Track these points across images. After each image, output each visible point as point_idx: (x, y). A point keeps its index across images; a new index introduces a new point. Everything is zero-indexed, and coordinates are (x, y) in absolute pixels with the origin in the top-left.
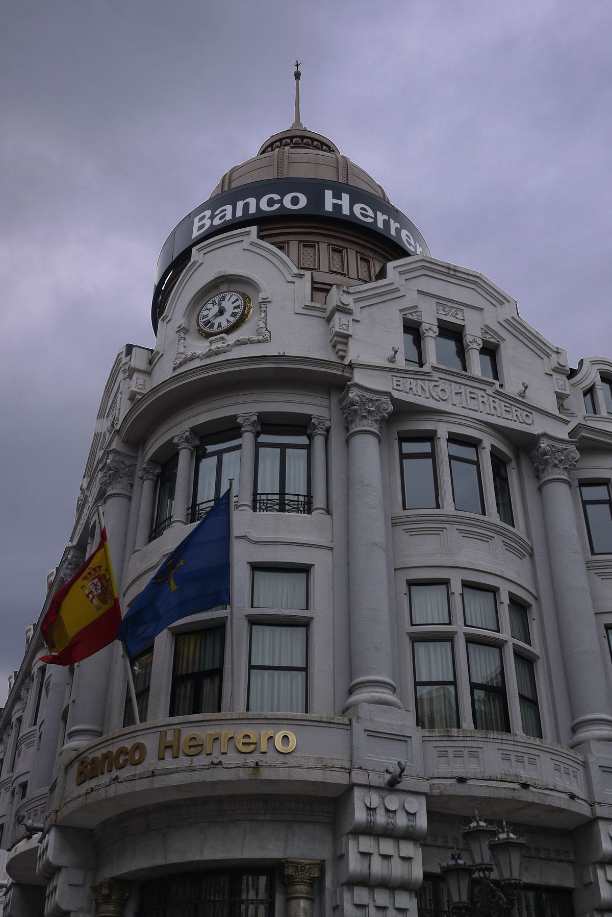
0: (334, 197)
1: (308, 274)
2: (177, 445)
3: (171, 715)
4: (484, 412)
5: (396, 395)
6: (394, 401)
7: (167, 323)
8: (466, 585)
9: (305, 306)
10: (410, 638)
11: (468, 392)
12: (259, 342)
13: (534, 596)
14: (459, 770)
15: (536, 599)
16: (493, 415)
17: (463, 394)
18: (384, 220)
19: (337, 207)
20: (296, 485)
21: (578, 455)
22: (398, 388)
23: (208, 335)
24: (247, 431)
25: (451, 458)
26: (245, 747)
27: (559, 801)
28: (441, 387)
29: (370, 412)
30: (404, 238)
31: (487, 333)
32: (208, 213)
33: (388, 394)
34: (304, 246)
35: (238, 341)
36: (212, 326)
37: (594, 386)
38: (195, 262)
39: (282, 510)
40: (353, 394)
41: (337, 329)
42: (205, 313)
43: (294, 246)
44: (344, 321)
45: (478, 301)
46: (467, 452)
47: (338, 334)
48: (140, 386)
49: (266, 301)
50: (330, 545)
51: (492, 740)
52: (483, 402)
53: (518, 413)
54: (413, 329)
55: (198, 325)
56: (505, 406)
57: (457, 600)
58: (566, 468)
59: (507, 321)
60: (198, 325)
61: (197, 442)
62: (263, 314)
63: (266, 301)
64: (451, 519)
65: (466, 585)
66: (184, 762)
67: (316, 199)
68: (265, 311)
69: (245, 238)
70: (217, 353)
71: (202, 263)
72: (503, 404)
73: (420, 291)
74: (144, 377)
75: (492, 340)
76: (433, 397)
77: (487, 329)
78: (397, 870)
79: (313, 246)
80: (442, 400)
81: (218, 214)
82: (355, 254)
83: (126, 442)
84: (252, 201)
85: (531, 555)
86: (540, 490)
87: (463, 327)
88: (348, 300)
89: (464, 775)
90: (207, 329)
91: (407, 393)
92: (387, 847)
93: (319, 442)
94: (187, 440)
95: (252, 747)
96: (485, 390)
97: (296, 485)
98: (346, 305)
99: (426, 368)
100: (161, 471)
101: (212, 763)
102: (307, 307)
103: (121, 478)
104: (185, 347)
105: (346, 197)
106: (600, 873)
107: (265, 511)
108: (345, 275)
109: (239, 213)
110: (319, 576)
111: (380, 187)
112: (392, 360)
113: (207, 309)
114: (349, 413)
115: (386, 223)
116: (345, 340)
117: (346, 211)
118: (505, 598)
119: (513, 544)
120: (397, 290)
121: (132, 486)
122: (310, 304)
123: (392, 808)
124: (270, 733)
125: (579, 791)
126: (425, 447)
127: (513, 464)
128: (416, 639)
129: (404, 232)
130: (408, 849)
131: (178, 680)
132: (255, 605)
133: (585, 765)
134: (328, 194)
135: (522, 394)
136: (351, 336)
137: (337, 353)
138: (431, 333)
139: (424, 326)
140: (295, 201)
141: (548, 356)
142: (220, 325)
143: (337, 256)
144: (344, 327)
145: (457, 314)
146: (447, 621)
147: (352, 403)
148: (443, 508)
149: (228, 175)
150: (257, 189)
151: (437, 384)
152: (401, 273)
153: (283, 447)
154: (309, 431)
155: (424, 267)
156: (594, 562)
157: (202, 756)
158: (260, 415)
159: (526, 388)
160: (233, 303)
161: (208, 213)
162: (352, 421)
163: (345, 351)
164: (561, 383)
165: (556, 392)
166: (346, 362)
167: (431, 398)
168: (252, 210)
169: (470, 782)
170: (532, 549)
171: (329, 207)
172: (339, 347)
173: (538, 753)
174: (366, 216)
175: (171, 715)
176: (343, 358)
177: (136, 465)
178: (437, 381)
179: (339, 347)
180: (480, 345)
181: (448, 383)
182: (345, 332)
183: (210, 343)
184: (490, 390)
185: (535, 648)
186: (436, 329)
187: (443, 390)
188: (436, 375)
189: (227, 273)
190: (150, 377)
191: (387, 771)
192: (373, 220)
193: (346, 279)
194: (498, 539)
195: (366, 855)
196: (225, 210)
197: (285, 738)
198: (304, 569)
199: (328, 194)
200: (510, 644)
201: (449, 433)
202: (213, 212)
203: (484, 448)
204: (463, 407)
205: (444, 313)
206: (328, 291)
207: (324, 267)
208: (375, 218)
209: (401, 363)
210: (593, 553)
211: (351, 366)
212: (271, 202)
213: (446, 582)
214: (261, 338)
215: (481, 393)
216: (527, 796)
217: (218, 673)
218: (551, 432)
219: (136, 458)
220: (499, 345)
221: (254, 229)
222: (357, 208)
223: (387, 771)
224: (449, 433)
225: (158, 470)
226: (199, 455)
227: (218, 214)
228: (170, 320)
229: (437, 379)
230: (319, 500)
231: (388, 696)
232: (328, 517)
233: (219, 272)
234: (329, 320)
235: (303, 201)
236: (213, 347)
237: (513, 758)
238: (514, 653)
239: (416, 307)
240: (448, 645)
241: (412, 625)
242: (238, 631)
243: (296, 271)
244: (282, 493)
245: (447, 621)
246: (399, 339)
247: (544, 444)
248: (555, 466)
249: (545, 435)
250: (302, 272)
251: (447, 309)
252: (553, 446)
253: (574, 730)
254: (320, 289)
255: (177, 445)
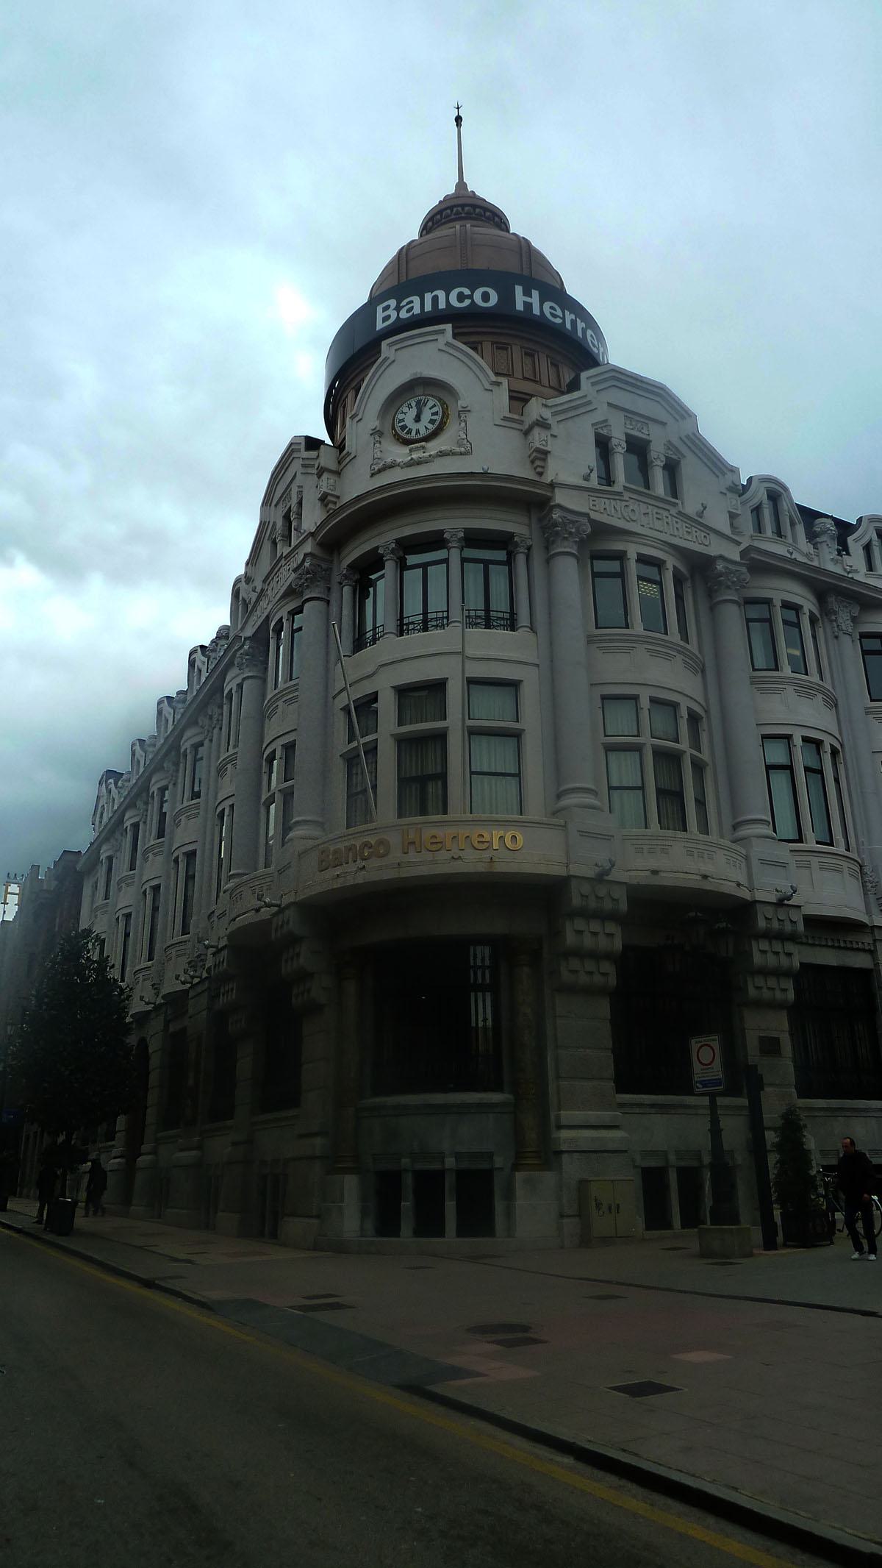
0: (525, 294)
1: (504, 381)
2: (382, 556)
3: (400, 816)
4: (668, 533)
5: (594, 516)
6: (592, 522)
7: (357, 422)
8: (654, 701)
9: (504, 417)
10: (604, 748)
11: (654, 513)
12: (461, 454)
13: (704, 708)
14: (653, 863)
15: (706, 711)
16: (676, 536)
17: (650, 516)
18: (572, 320)
19: (528, 306)
20: (500, 603)
21: (748, 577)
22: (594, 508)
23: (407, 442)
24: (454, 547)
25: (640, 578)
26: (481, 844)
27: (728, 888)
28: (631, 508)
29: (571, 533)
30: (589, 338)
31: (669, 449)
32: (393, 303)
33: (587, 515)
34: (498, 348)
35: (441, 452)
36: (410, 432)
37: (761, 503)
38: (386, 359)
39: (488, 626)
40: (556, 515)
41: (537, 445)
42: (401, 416)
43: (487, 347)
44: (543, 436)
45: (663, 416)
46: (651, 572)
47: (538, 450)
48: (332, 487)
49: (466, 410)
50: (536, 662)
51: (679, 839)
52: (667, 523)
53: (697, 534)
54: (603, 445)
55: (393, 428)
56: (686, 527)
57: (645, 715)
58: (737, 590)
59: (688, 437)
60: (393, 428)
61: (401, 554)
62: (463, 424)
63: (466, 410)
64: (640, 639)
65: (654, 701)
66: (429, 856)
67: (507, 297)
68: (465, 421)
69: (439, 337)
70: (419, 463)
71: (394, 361)
72: (684, 524)
73: (611, 404)
74: (333, 479)
75: (673, 456)
76: (624, 518)
77: (669, 445)
78: (603, 943)
79: (506, 349)
80: (633, 521)
81: (404, 306)
82: (546, 358)
83: (321, 545)
84: (441, 294)
85: (703, 671)
86: (712, 609)
87: (649, 442)
88: (547, 414)
89: (655, 868)
90: (403, 434)
91: (601, 513)
92: (595, 926)
93: (521, 559)
94: (393, 551)
95: (486, 845)
96: (669, 510)
97: (500, 603)
98: (546, 420)
99: (618, 487)
100: (359, 577)
101: (453, 858)
102: (505, 419)
103: (319, 581)
104: (381, 451)
105: (535, 293)
106: (754, 943)
107: (474, 627)
108: (537, 381)
109: (428, 307)
110: (530, 692)
111: (558, 273)
112: (587, 478)
113: (403, 413)
114: (550, 534)
115: (574, 323)
116: (543, 456)
117: (536, 311)
118: (684, 713)
119: (664, 650)
120: (589, 403)
121: (329, 589)
122: (508, 415)
123: (601, 895)
124: (501, 833)
125: (743, 880)
126: (614, 566)
127: (689, 584)
128: (610, 748)
129: (589, 332)
130: (612, 928)
131: (403, 782)
132: (471, 717)
133: (747, 858)
134: (519, 290)
135: (701, 514)
136: (549, 452)
137: (535, 469)
138: (620, 449)
139: (614, 441)
140: (486, 297)
141: (724, 474)
142: (418, 432)
143: (528, 361)
144: (544, 443)
145: (642, 428)
146: (636, 733)
147: (555, 525)
148: (633, 628)
149: (404, 250)
150: (446, 280)
151: (627, 504)
152: (593, 384)
153: (486, 563)
154: (510, 548)
155: (614, 378)
156: (755, 677)
157: (443, 851)
158: (467, 531)
159: (705, 508)
160: (430, 409)
161: (393, 303)
162: (553, 542)
163: (543, 467)
164: (734, 502)
165: (729, 512)
166: (548, 480)
167: (623, 519)
168: (442, 305)
169: (663, 874)
170: (704, 665)
171: (520, 307)
172: (538, 463)
173: (714, 849)
174: (555, 316)
175: (400, 816)
176: (540, 474)
177: (331, 569)
178: (627, 501)
179: (538, 463)
180: (662, 461)
181: (637, 503)
182: (545, 448)
183: (410, 451)
184: (673, 511)
185: (705, 756)
186: (624, 445)
187: (633, 510)
188: (627, 495)
189: (423, 376)
190: (340, 477)
191: (596, 865)
192: (561, 321)
193: (537, 387)
194: (679, 657)
195: (579, 932)
196: (412, 302)
197: (514, 837)
198: (514, 685)
199: (519, 290)
200: (688, 754)
201: (638, 554)
202: (398, 303)
203: (667, 569)
204: (650, 528)
205: (631, 427)
206: (526, 401)
207: (518, 374)
208: (564, 318)
209: (594, 482)
210: (754, 670)
211: (552, 486)
212: (461, 297)
213: (635, 698)
214: (463, 449)
215: (665, 513)
216: (707, 886)
217: (442, 777)
218: (726, 554)
219: (332, 562)
220: (680, 461)
221: (448, 327)
222: (547, 305)
223: (596, 865)
224: (638, 554)
225: (357, 577)
226: (403, 566)
227: (404, 306)
228: (361, 419)
229: (627, 499)
230: (523, 618)
231: (590, 800)
232: (532, 635)
233: (416, 374)
234: (526, 433)
235: (494, 299)
236: (415, 456)
237: (696, 855)
238: (691, 763)
239: (606, 421)
240: (637, 754)
241: (606, 736)
242: (455, 743)
243: (494, 378)
244: (487, 609)
245: (636, 733)
246: (590, 456)
247: (720, 566)
248: (728, 587)
249: (721, 557)
250: (500, 379)
251: (634, 423)
252: (727, 568)
253: (735, 827)
254: (520, 399)
255: (382, 556)
